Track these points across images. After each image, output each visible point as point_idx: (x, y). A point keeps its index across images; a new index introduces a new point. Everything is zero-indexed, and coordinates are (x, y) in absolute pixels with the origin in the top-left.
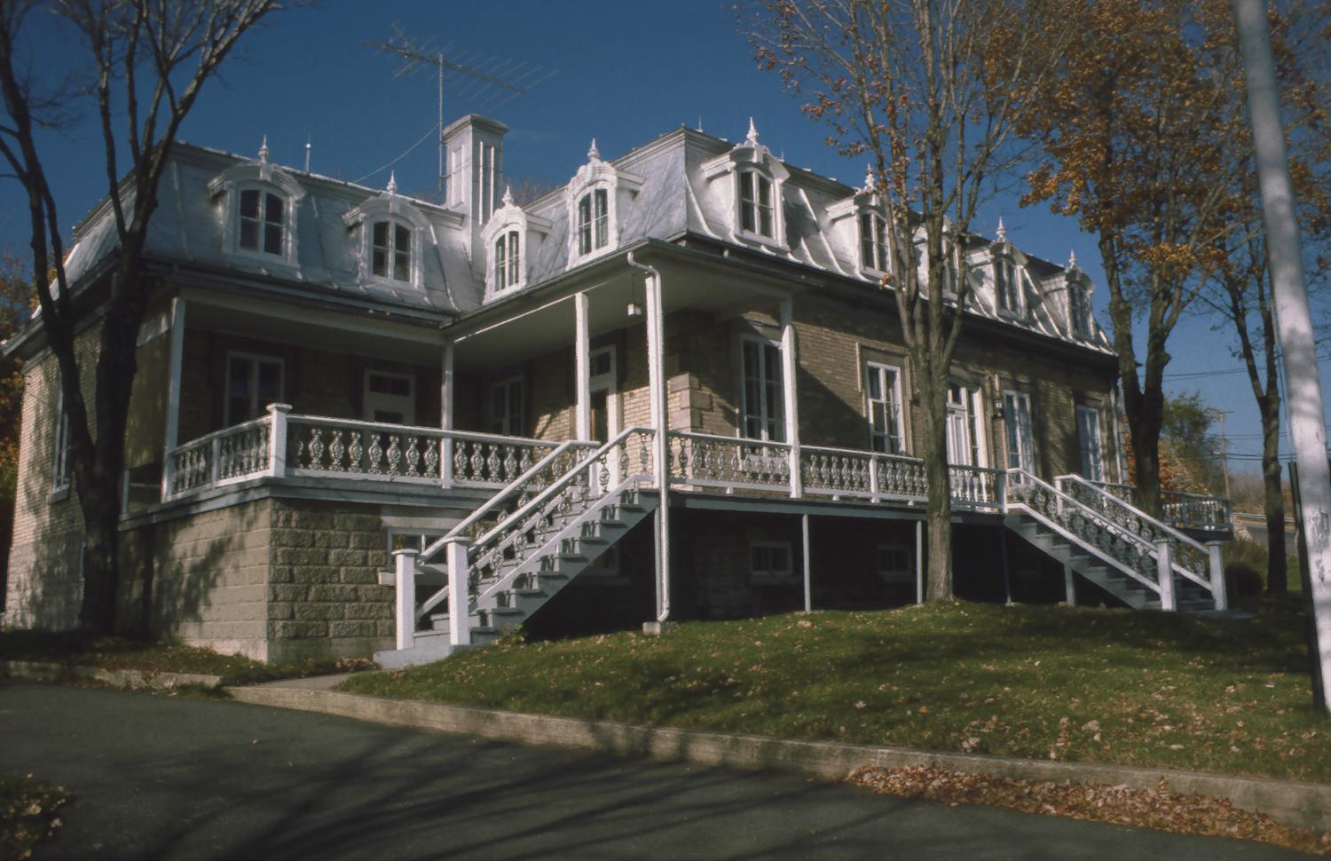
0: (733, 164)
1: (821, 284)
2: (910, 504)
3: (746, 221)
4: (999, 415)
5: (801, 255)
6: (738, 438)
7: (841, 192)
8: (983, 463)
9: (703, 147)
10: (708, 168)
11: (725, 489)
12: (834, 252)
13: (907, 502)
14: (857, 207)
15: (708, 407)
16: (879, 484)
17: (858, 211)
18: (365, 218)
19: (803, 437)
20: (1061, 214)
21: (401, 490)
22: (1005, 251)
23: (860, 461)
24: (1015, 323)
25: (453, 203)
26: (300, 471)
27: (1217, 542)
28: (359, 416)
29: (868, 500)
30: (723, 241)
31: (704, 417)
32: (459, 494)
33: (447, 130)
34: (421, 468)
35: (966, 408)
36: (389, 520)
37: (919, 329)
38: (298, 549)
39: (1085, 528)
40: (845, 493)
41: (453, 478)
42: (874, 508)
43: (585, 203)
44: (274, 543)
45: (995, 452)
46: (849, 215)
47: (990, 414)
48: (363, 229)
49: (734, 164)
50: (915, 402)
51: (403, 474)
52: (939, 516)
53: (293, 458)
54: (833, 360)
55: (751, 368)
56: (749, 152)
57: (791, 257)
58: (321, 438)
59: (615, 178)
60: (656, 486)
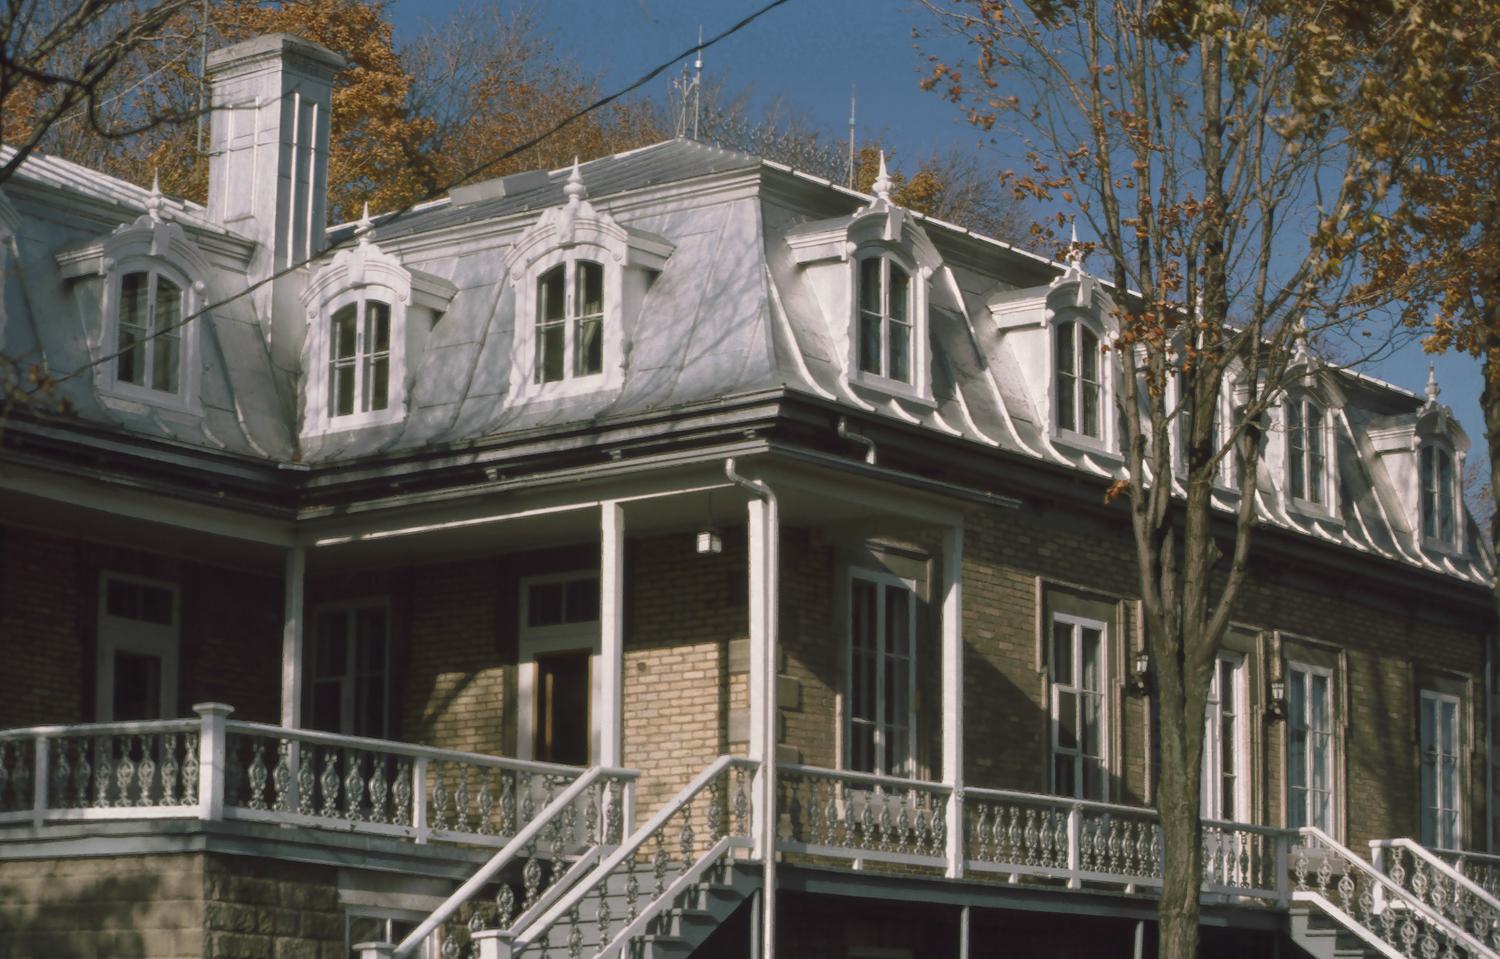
3: (866, 359)
4: (1278, 711)
5: (953, 417)
6: (838, 769)
7: (1025, 276)
8: (1242, 814)
9: (795, 203)
10: (805, 245)
11: (851, 861)
12: (1006, 400)
13: (1122, 887)
14: (1051, 313)
15: (794, 705)
16: (1081, 856)
17: (1052, 321)
18: (111, 269)
19: (969, 774)
21: (369, 844)
22: (1308, 381)
23: (1038, 815)
25: (227, 214)
26: (242, 813)
28: (334, 728)
29: (1062, 882)
31: (790, 723)
32: (443, 854)
33: (217, 57)
34: (389, 810)
35: (1218, 699)
36: (348, 895)
37: (1167, 581)
38: (237, 936)
39: (1419, 940)
40: (1029, 870)
41: (429, 826)
42: (1073, 897)
43: (553, 281)
44: (208, 924)
45: (1266, 785)
46: (1037, 325)
47: (1261, 711)
49: (852, 246)
50: (1130, 690)
52: (1179, 915)
53: (235, 790)
54: (996, 613)
55: (864, 633)
56: (878, 220)
59: (622, 249)
60: (757, 855)
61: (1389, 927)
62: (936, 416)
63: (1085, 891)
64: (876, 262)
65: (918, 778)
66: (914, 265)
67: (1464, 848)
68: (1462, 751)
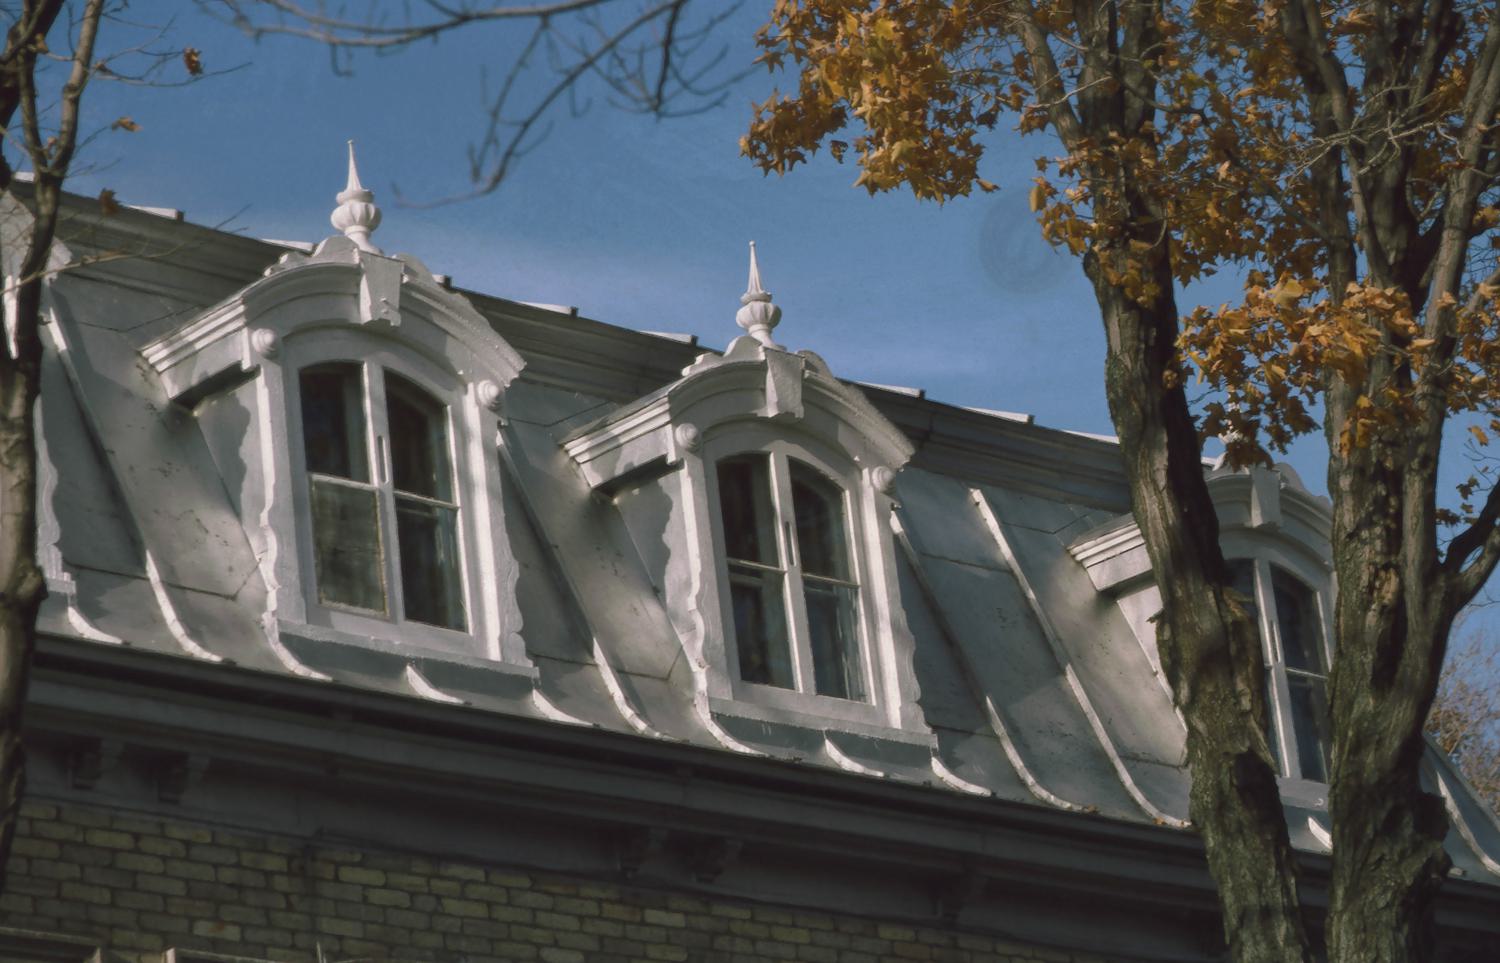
0: (684, 434)
20: (402, 272)
24: (833, 753)
30: (596, 732)
49: (263, 338)
57: (541, 706)
66: (850, 468)
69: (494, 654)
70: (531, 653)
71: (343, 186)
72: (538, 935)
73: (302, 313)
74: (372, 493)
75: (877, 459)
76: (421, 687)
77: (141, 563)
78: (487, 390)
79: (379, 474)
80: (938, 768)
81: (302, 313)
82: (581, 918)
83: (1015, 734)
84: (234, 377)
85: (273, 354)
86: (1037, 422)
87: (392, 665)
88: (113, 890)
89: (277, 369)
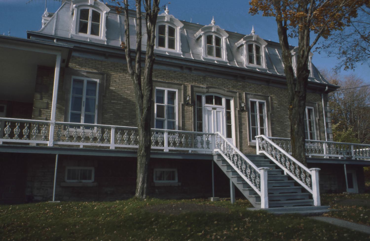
1: (71, 46)
2: (339, 158)
27: (314, 169)
47: (238, 109)
48: (245, 46)
49: (245, 41)
51: (157, 146)
52: (139, 155)
56: (211, 28)
58: (10, 126)
61: (231, 157)
62: (315, 80)
63: (4, 145)
64: (252, 45)
65: (317, 140)
66: (261, 45)
67: (179, 129)
68: (315, 119)
69: (264, 67)
70: (228, 60)
71: (212, 20)
72: (227, 84)
73: (207, 30)
74: (213, 46)
75: (225, 36)
76: (258, 70)
77: (190, 51)
78: (179, 27)
79: (214, 44)
80: (268, 71)
81: (207, 30)
82: (232, 83)
83: (276, 69)
84: (242, 45)
85: (204, 34)
86: (186, 21)
87: (214, 60)
88: (185, 79)
89: (246, 44)
